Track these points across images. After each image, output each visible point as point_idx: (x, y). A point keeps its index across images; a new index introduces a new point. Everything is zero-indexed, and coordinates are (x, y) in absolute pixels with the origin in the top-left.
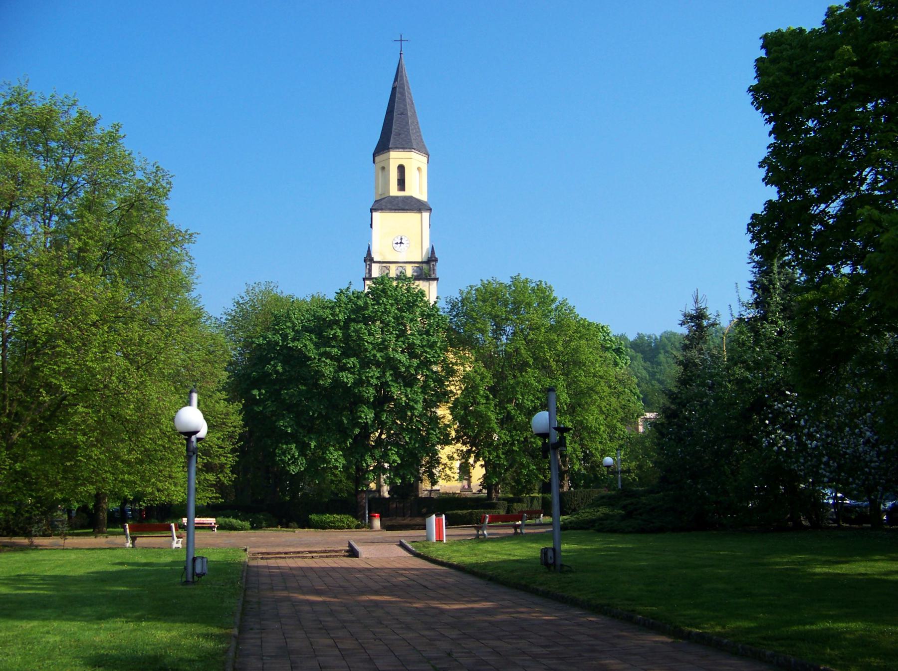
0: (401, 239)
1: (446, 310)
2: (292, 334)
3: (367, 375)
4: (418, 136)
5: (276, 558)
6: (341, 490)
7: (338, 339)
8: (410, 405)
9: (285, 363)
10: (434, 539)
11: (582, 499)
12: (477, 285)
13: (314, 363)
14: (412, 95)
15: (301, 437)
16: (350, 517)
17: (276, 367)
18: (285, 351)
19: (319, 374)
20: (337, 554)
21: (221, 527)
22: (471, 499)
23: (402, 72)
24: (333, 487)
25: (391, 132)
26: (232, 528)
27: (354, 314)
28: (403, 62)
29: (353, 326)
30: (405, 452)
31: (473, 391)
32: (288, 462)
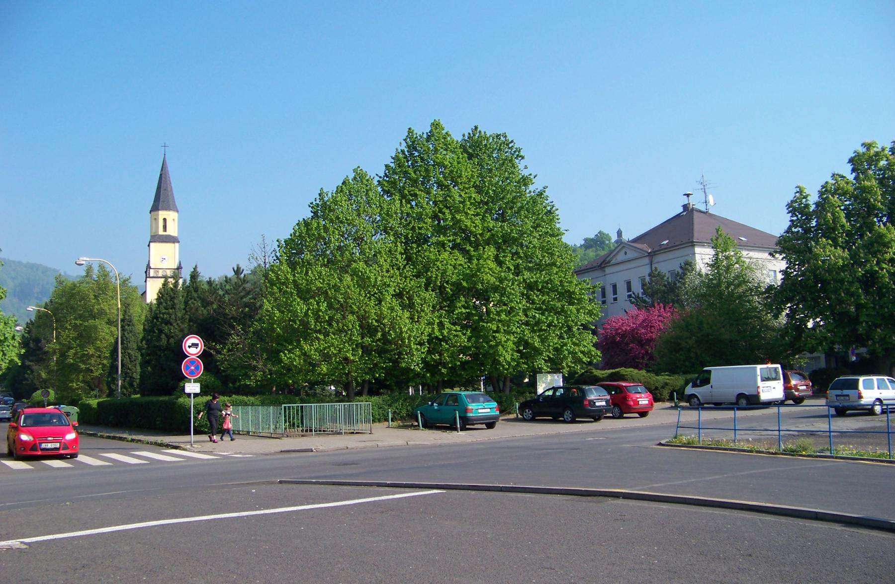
28: (168, 161)
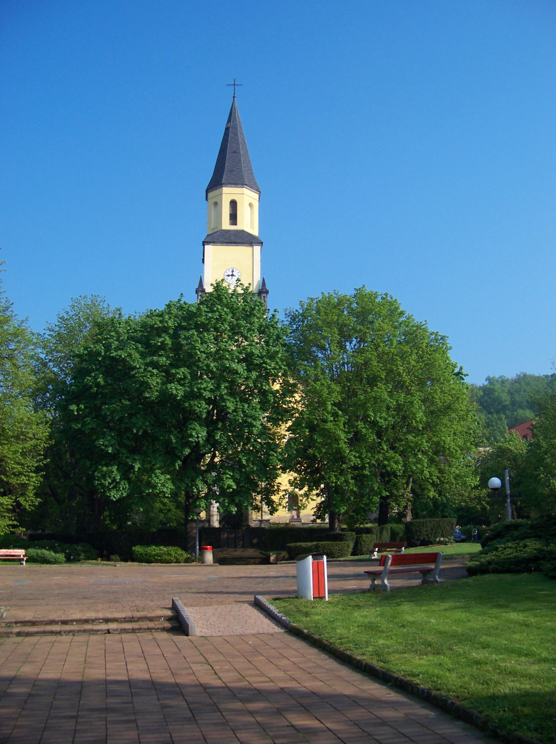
0: (233, 271)
1: (285, 323)
2: (116, 343)
3: (199, 386)
4: (250, 174)
5: (44, 633)
6: (170, 520)
7: (167, 348)
8: (248, 422)
9: (107, 373)
10: (311, 594)
11: (432, 530)
12: (318, 298)
13: (139, 372)
14: (245, 135)
15: (124, 458)
16: (179, 549)
17: (96, 379)
18: (107, 362)
19: (145, 386)
20: (151, 625)
21: (31, 560)
22: (305, 530)
23: (235, 114)
24: (161, 516)
25: (224, 169)
26: (45, 561)
27: (185, 321)
28: (237, 104)
29: (183, 334)
30: (241, 476)
31: (319, 407)
32: (108, 487)
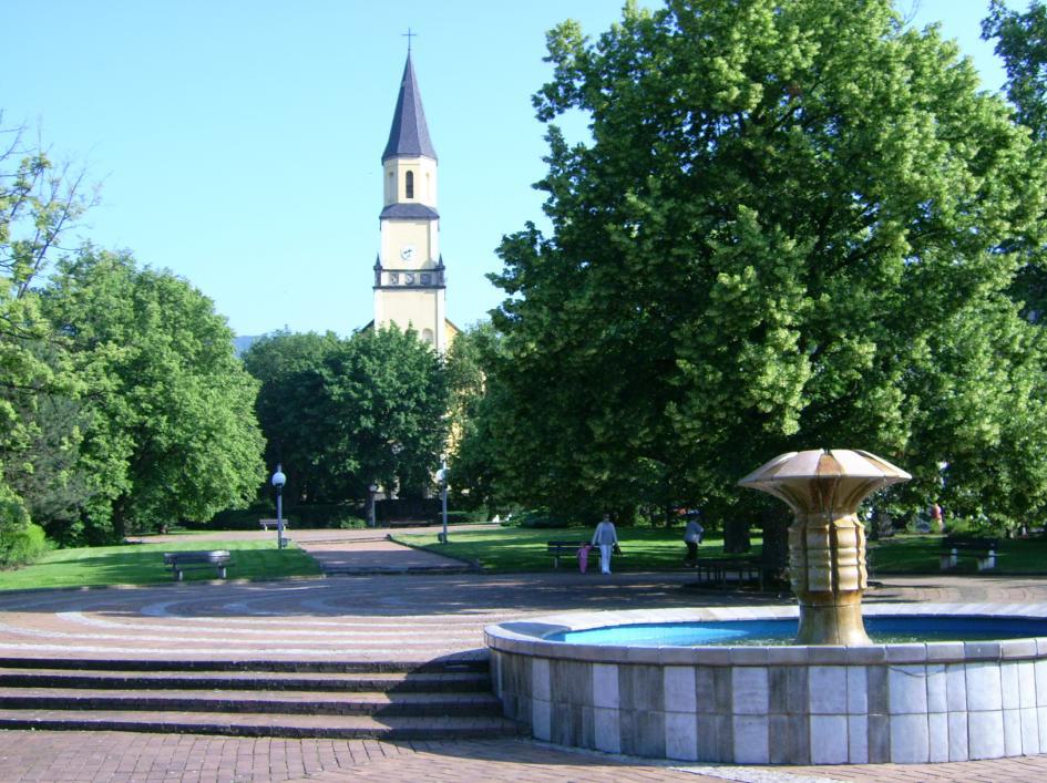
28: (412, 59)
